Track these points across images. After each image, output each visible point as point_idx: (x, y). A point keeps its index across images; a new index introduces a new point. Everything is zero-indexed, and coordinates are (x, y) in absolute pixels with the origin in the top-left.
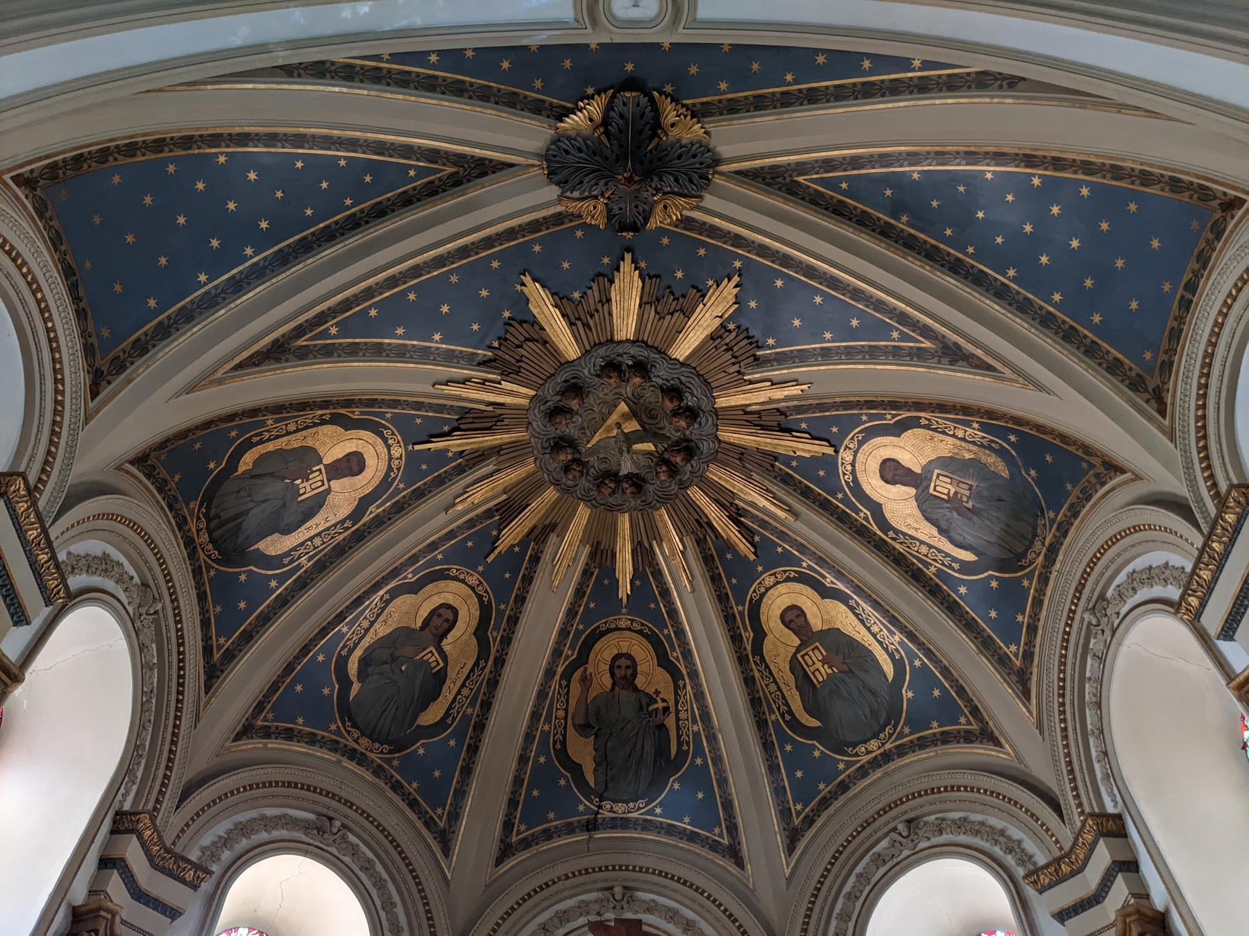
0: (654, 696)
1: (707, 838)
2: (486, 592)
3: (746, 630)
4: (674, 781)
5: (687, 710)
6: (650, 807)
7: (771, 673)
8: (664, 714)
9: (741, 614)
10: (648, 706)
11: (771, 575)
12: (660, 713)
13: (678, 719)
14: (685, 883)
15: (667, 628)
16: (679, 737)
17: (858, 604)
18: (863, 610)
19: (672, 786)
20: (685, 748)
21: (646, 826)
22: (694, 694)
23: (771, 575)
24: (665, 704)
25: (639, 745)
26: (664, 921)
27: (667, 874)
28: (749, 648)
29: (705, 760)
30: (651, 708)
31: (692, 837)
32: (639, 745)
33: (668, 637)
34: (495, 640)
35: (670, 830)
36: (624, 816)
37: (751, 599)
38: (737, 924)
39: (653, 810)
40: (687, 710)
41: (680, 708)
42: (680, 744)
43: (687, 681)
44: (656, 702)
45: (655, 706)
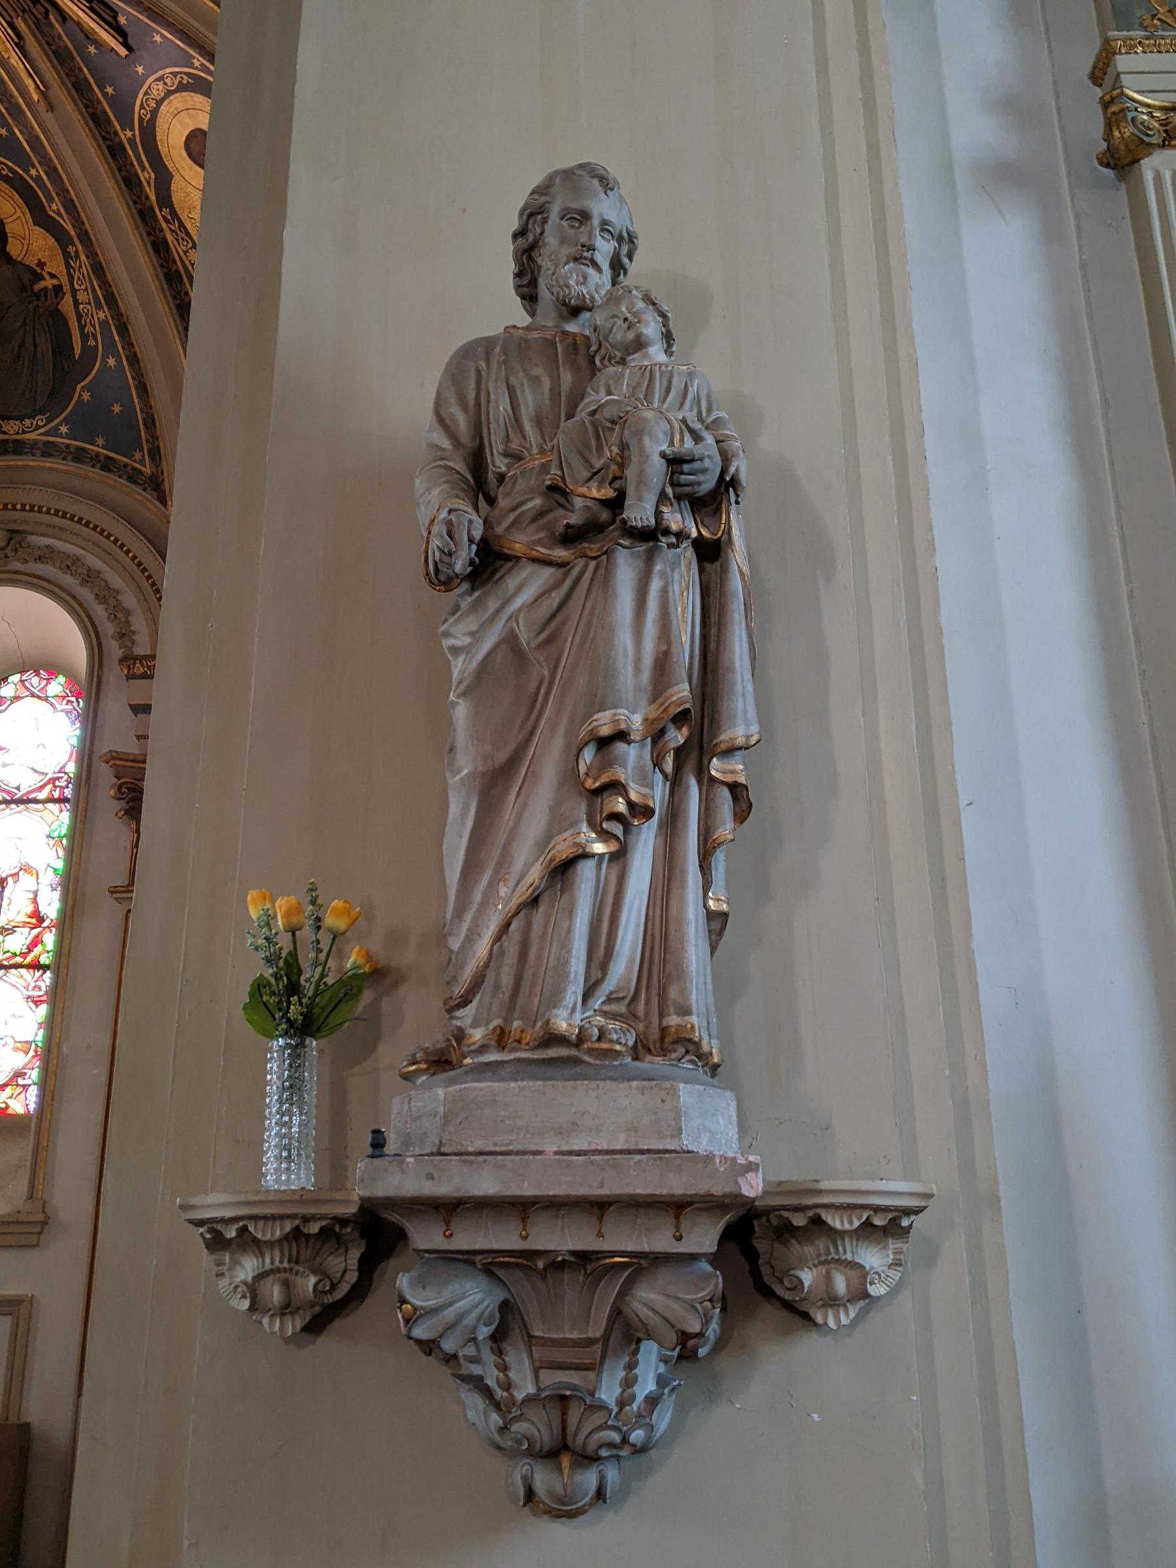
0: (38, 270)
1: (126, 466)
2: (175, 74)
3: (143, 169)
4: (82, 389)
5: (86, 290)
6: (52, 425)
7: (188, 233)
8: (56, 297)
9: (132, 141)
10: (33, 284)
11: (158, 80)
12: (50, 295)
13: (76, 304)
14: (87, 525)
15: (34, 167)
16: (82, 328)
17: (77, 256)
18: (80, 266)
19: (80, 395)
20: (92, 343)
21: (48, 450)
22: (91, 266)
23: (158, 80)
24: (55, 282)
25: (29, 339)
26: (58, 571)
27: (65, 514)
28: (153, 198)
29: (119, 361)
30: (37, 287)
31: (107, 465)
32: (29, 339)
33: (38, 180)
34: (58, 213)
35: (80, 456)
36: (18, 437)
37: (141, 120)
38: (146, 574)
39: (56, 428)
40: (86, 290)
41: (77, 287)
42: (84, 337)
43: (80, 248)
44: (44, 279)
45: (42, 284)
